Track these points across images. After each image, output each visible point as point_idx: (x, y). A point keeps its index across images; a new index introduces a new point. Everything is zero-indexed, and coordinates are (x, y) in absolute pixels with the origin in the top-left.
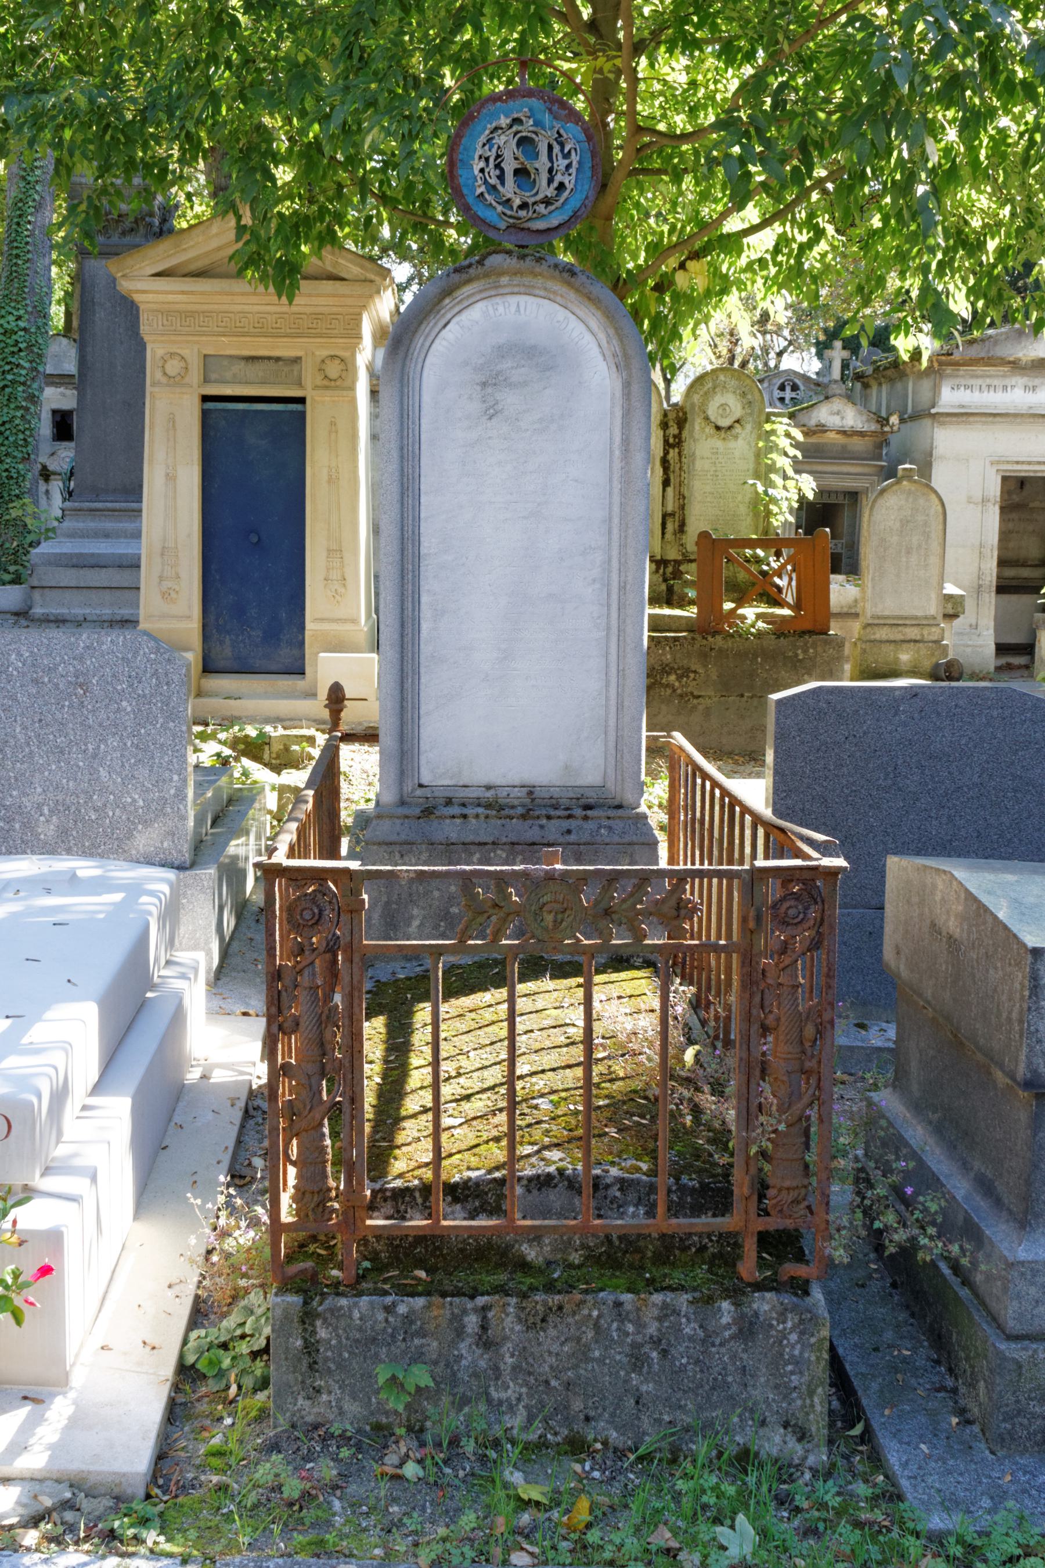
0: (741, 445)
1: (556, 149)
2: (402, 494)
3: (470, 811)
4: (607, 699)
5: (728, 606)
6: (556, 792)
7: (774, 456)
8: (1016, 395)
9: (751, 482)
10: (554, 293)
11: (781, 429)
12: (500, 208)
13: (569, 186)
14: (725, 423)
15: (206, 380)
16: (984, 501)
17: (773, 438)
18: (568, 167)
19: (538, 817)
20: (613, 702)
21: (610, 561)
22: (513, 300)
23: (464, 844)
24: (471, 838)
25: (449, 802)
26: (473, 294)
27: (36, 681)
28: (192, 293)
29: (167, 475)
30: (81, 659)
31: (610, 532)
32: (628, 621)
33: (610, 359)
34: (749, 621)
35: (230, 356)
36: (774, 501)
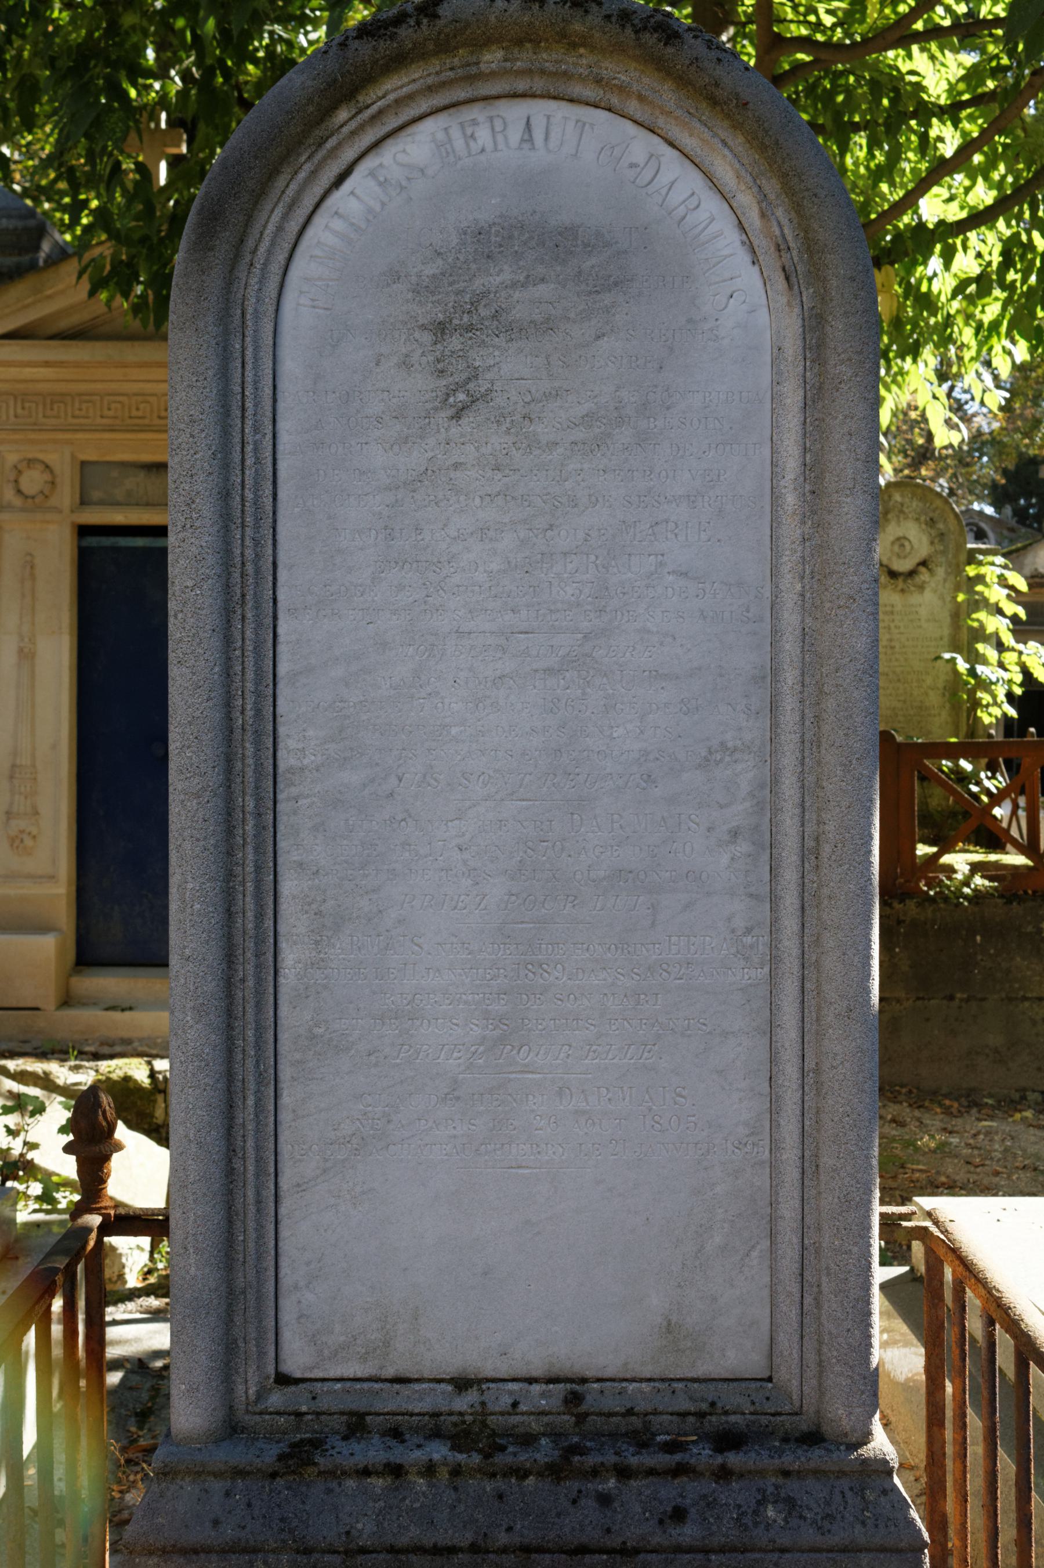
0: (929, 601)
2: (227, 614)
3: (413, 1456)
4: (775, 1146)
5: (923, 850)
6: (641, 1396)
7: (982, 615)
9: (947, 656)
10: (622, 89)
11: (991, 573)
14: (903, 566)
15: (84, 502)
17: (979, 588)
19: (595, 1472)
20: (790, 1155)
21: (775, 780)
22: (515, 112)
23: (392, 1550)
24: (412, 1534)
25: (357, 1425)
26: (411, 97)
28: (60, 364)
29: (21, 650)
31: (774, 707)
32: (829, 941)
33: (769, 259)
34: (959, 876)
35: (123, 465)
36: (986, 685)
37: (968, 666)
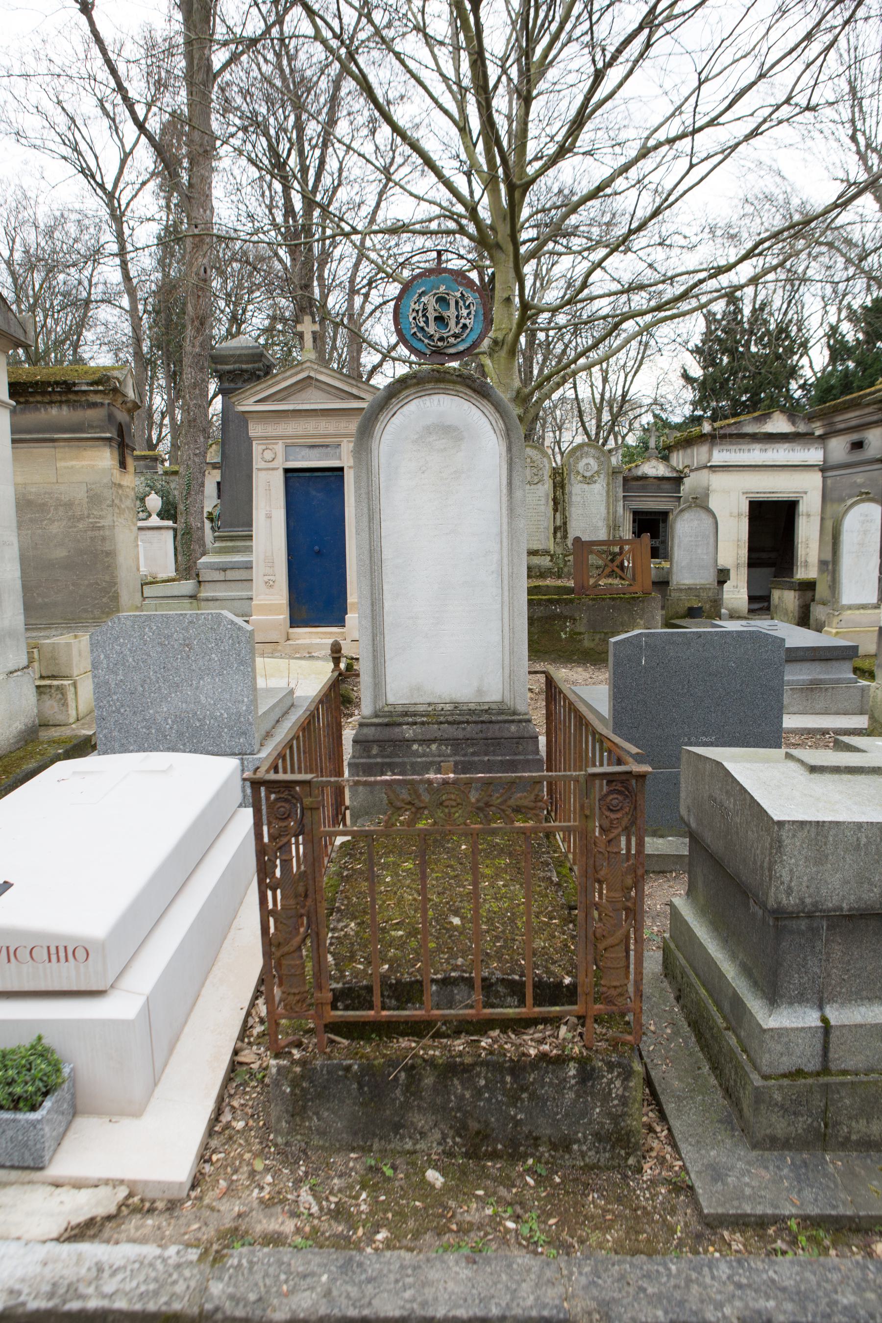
1: (461, 303)
8: (755, 454)
12: (426, 341)
13: (470, 327)
16: (739, 515)
18: (469, 314)
25: (406, 714)
27: (160, 644)
30: (186, 629)
37: (681, 405)
